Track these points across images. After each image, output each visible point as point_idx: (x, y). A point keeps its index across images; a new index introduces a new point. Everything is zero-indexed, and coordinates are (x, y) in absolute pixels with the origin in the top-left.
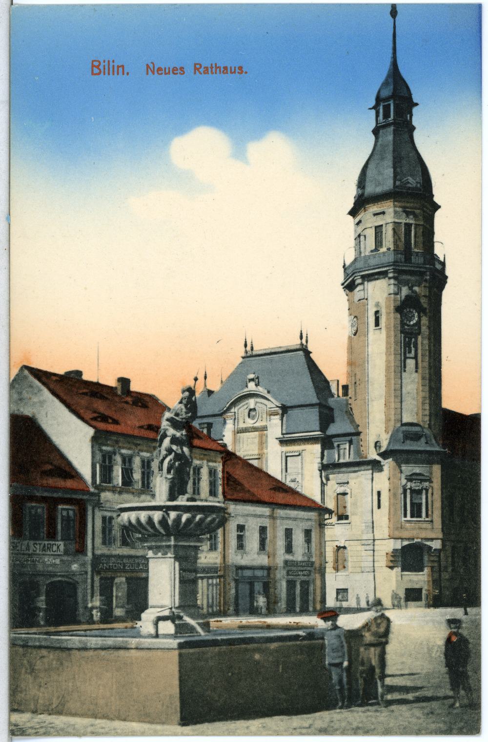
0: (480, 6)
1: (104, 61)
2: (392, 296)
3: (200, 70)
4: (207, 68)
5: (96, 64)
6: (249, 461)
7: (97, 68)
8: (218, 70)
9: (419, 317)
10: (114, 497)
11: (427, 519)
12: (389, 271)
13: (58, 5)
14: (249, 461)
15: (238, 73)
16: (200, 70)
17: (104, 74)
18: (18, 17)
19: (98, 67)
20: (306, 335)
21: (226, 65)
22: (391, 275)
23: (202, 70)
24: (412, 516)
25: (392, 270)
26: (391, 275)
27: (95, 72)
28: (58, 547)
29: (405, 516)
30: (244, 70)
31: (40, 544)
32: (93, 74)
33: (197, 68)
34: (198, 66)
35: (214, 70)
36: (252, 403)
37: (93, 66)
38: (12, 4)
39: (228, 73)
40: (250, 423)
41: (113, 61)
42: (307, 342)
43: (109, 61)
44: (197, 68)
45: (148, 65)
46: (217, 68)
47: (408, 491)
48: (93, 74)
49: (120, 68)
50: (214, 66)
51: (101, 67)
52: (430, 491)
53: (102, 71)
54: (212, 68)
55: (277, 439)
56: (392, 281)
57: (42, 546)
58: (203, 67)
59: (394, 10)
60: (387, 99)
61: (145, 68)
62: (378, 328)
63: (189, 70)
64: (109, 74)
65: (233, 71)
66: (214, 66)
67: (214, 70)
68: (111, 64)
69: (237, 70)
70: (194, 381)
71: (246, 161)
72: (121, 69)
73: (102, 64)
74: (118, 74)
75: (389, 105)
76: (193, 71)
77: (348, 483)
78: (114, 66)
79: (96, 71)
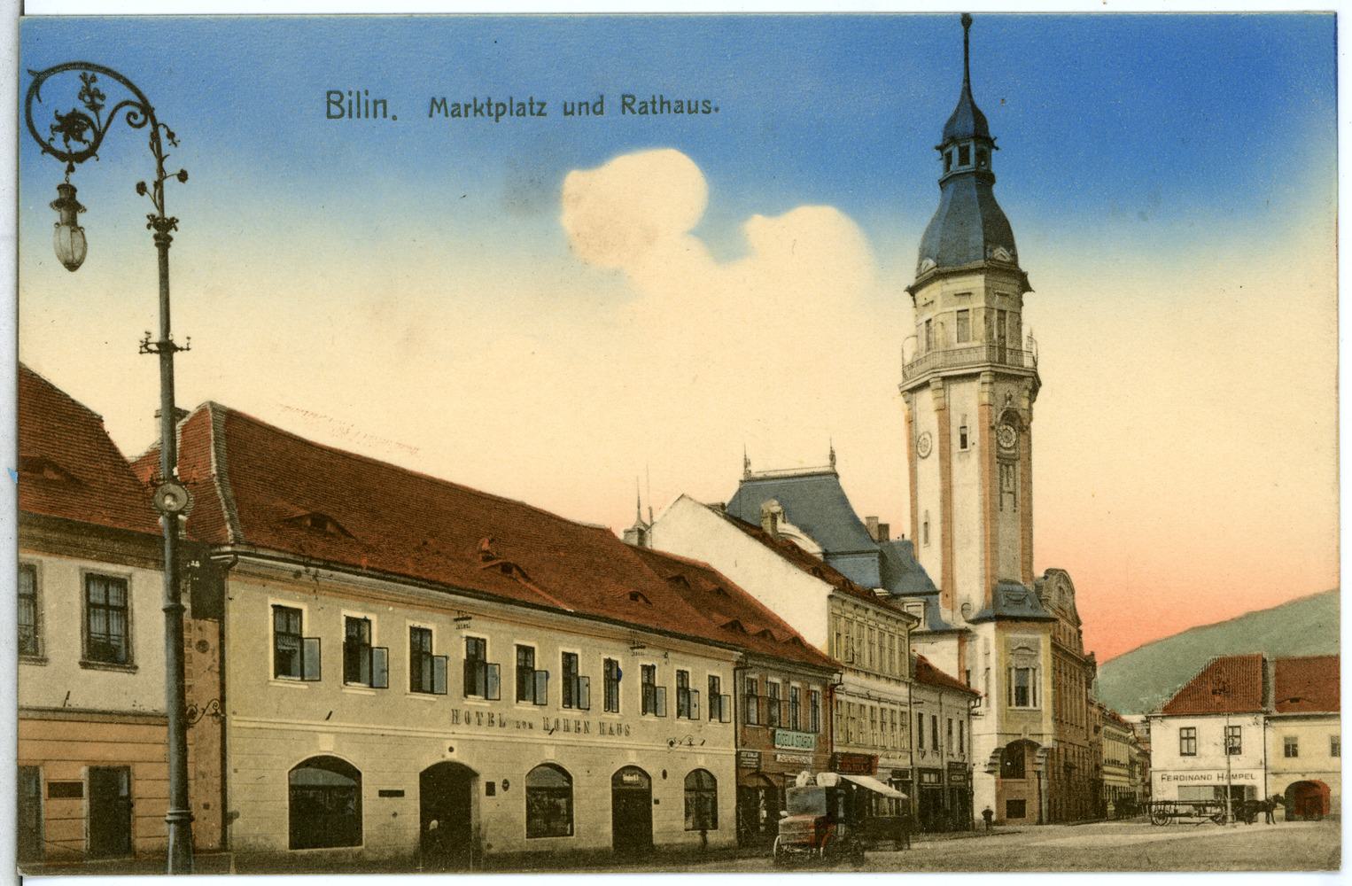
0: (1336, 15)
1: (350, 93)
2: (987, 407)
3: (633, 107)
4: (522, 105)
5: (335, 97)
7: (336, 104)
8: (665, 106)
9: (1017, 436)
10: (983, 764)
12: (983, 374)
15: (704, 112)
16: (341, 104)
17: (350, 116)
18: (31, 32)
19: (337, 104)
23: (636, 107)
24: (1017, 704)
25: (988, 373)
27: (332, 113)
29: (1010, 705)
30: (712, 105)
32: (329, 116)
34: (629, 100)
35: (658, 107)
37: (329, 102)
38: (22, 13)
39: (682, 112)
41: (367, 93)
43: (358, 93)
44: (626, 103)
45: (433, 100)
46: (662, 103)
47: (1013, 671)
48: (329, 116)
49: (378, 106)
50: (657, 99)
51: (345, 104)
52: (1038, 671)
53: (508, 109)
54: (654, 103)
59: (966, 20)
60: (966, 138)
61: (429, 101)
62: (965, 450)
63: (553, 110)
64: (367, 115)
65: (693, 107)
66: (657, 99)
67: (658, 107)
68: (363, 96)
69: (701, 107)
71: (148, 217)
72: (380, 107)
73: (347, 97)
74: (375, 116)
75: (968, 147)
76: (427, 110)
78: (367, 102)
79: (335, 110)
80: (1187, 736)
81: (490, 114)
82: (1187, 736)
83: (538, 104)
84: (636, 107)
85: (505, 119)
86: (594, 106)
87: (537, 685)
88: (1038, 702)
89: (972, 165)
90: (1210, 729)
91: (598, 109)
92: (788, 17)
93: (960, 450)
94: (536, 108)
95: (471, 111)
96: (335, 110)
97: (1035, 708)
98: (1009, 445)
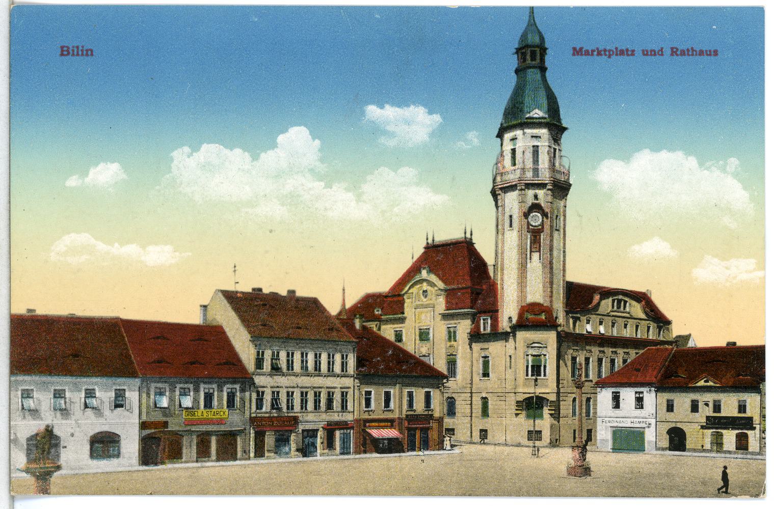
6: (646, 318)
11: (544, 378)
13: (559, 8)
14: (646, 318)
20: (470, 231)
21: (719, 54)
22: (549, 187)
23: (679, 53)
26: (549, 187)
28: (224, 413)
29: (527, 375)
31: (211, 411)
33: (674, 52)
34: (675, 50)
36: (425, 286)
40: (424, 301)
42: (471, 235)
55: (440, 314)
56: (549, 192)
57: (212, 413)
58: (679, 51)
63: (667, 52)
70: (234, 273)
77: (488, 349)
80: (616, 399)
81: (606, 55)
82: (616, 399)
83: (631, 51)
84: (679, 53)
85: (614, 57)
86: (658, 52)
87: (602, 313)
88: (405, 399)
89: (534, 78)
90: (628, 395)
91: (660, 53)
92: (177, 6)
93: (509, 229)
94: (630, 53)
95: (595, 53)
96: (65, 53)
97: (544, 378)
98: (537, 224)
